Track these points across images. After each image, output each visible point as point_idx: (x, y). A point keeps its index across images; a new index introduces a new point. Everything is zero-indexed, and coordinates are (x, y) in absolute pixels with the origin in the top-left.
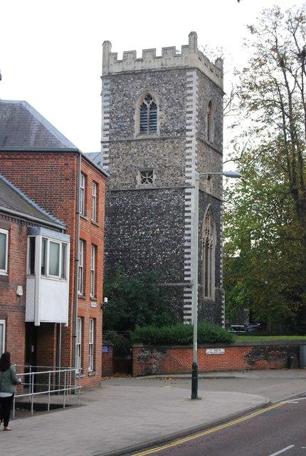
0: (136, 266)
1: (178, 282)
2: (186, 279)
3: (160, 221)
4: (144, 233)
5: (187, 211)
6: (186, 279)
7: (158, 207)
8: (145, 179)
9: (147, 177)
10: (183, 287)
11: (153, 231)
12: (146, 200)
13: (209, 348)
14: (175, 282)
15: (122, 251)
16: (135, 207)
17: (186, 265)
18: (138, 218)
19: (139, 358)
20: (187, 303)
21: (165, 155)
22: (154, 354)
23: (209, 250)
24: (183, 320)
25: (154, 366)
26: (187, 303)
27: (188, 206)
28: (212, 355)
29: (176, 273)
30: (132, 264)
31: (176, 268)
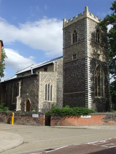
7: (78, 66)
10: (85, 93)
30: (71, 86)
31: (83, 86)
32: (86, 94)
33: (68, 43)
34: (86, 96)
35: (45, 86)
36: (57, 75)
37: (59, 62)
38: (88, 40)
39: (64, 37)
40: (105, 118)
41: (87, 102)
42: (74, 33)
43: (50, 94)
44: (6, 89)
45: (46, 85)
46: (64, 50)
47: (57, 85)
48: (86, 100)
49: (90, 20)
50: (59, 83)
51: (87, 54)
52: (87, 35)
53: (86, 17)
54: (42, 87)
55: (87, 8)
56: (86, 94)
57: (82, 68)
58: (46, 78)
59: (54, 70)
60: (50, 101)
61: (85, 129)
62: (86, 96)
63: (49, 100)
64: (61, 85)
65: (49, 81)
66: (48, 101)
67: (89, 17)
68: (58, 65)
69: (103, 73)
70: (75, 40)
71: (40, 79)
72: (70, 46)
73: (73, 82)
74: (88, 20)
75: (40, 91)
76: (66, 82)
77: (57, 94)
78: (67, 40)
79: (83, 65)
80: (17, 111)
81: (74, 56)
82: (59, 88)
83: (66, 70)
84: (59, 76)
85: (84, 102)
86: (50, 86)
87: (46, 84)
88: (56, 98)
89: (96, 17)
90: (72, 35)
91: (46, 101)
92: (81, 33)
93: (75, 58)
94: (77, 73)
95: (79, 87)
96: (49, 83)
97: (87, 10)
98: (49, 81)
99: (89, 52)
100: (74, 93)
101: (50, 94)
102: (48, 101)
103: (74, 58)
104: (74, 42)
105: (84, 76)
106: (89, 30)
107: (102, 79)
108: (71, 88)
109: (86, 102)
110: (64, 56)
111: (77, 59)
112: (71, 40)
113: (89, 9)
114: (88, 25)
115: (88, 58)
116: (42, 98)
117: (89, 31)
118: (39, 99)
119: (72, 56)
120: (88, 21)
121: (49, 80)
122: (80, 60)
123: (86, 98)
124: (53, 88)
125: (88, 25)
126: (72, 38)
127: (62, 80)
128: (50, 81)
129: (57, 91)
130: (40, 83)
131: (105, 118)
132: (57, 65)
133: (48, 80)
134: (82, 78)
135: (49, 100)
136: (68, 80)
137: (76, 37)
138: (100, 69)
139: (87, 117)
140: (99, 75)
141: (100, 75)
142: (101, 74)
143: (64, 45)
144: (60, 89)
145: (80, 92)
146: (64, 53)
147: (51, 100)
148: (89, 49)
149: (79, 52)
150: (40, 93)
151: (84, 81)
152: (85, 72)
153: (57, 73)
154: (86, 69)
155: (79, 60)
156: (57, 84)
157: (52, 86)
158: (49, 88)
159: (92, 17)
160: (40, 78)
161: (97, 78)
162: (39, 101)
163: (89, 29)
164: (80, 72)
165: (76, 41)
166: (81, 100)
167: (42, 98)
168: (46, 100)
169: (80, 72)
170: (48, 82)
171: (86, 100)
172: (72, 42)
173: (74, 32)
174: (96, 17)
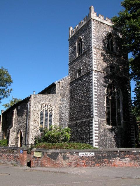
10: (90, 120)
36: (60, 98)
37: (63, 81)
38: (93, 48)
41: (92, 133)
44: (8, 120)
45: (42, 112)
46: (69, 66)
47: (60, 112)
49: (97, 23)
50: (63, 109)
51: (92, 66)
52: (93, 41)
53: (90, 20)
54: (35, 114)
55: (92, 7)
58: (42, 102)
59: (57, 92)
61: (63, 173)
64: (66, 113)
65: (47, 107)
67: (95, 18)
68: (62, 86)
69: (121, 92)
71: (32, 105)
74: (92, 22)
75: (31, 121)
77: (59, 124)
80: (9, 146)
82: (62, 116)
84: (62, 99)
87: (50, 112)
89: (107, 19)
95: (84, 113)
97: (93, 10)
98: (47, 107)
99: (96, 63)
105: (89, 97)
106: (95, 35)
113: (94, 9)
114: (93, 29)
115: (93, 71)
116: (36, 129)
117: (95, 36)
118: (31, 130)
120: (94, 24)
121: (47, 105)
125: (93, 29)
127: (67, 106)
128: (49, 107)
129: (60, 120)
130: (32, 109)
132: (60, 86)
136: (72, 105)
139: (88, 155)
140: (113, 95)
144: (63, 118)
148: (95, 59)
150: (31, 123)
152: (90, 91)
153: (60, 96)
154: (91, 87)
157: (51, 113)
158: (46, 115)
159: (101, 19)
160: (32, 102)
162: (30, 134)
163: (95, 34)
170: (44, 108)
174: (107, 19)
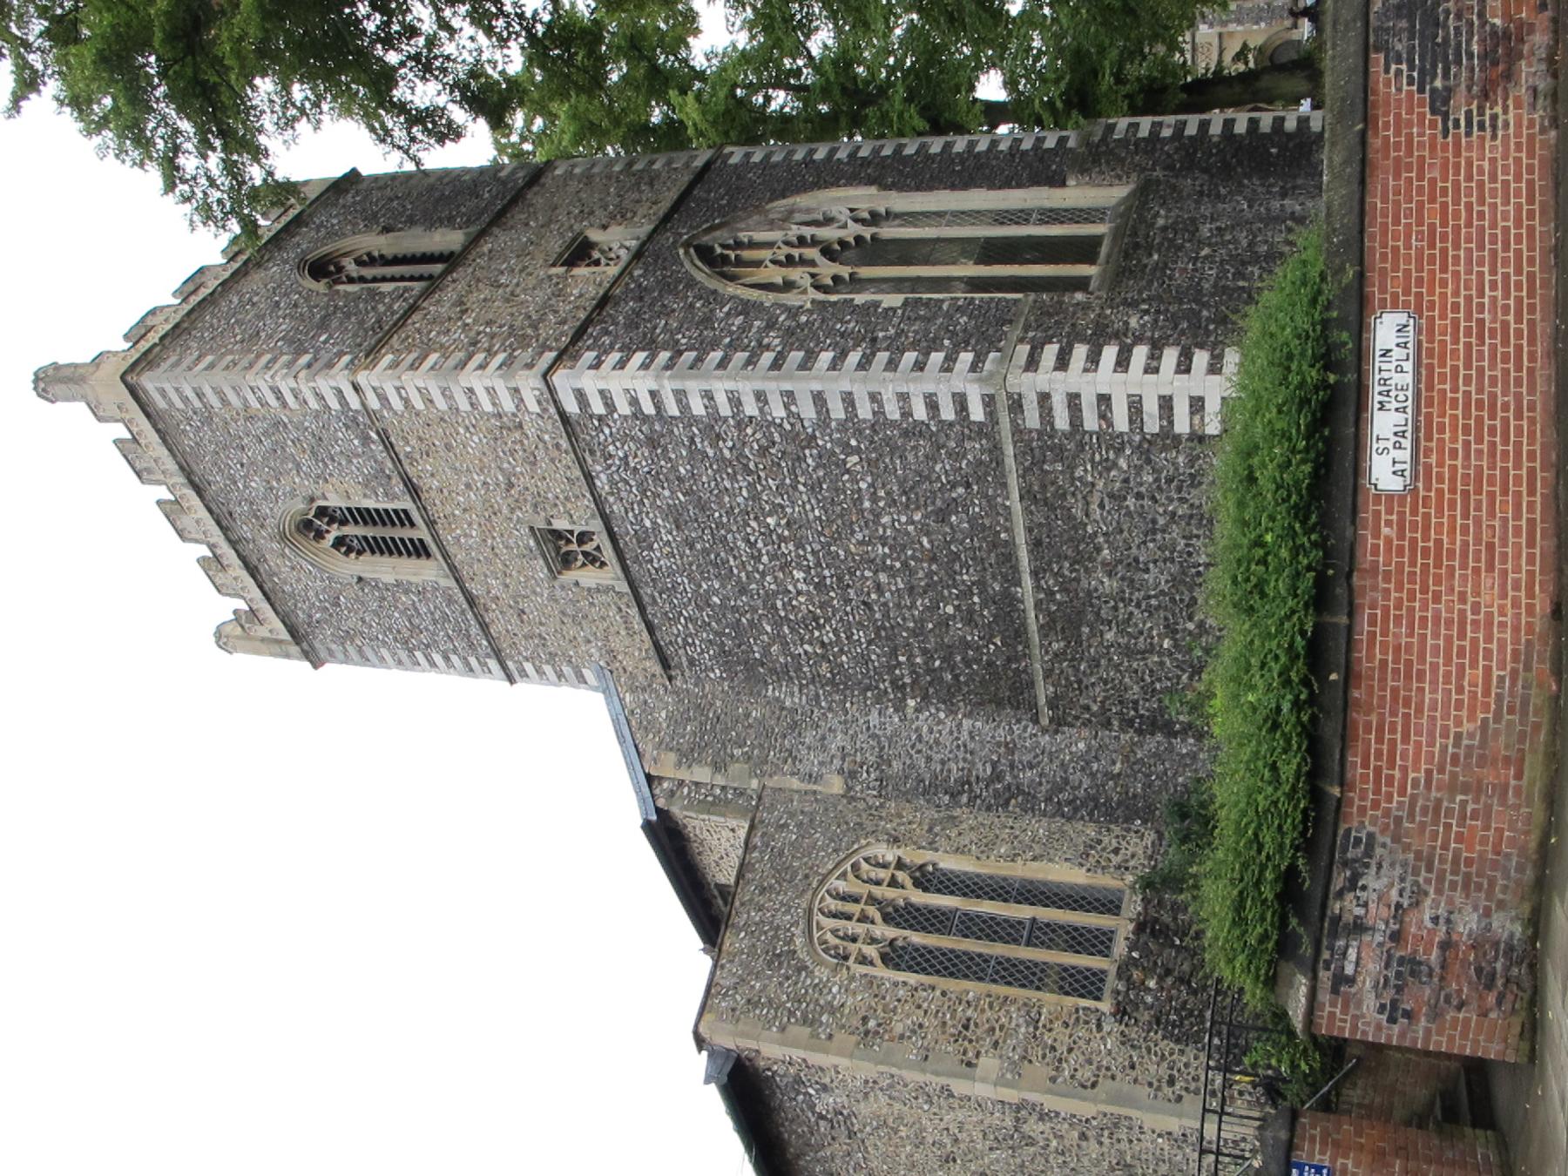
0: (950, 610)
1: (996, 448)
2: (977, 413)
3: (730, 512)
4: (799, 575)
5: (658, 406)
6: (977, 413)
7: (677, 518)
8: (585, 554)
9: (574, 547)
10: (1017, 431)
11: (782, 539)
12: (659, 558)
13: (1358, 467)
14: (1000, 463)
15: (894, 653)
16: (703, 601)
17: (906, 414)
18: (743, 590)
19: (1393, 1012)
20: (1104, 416)
21: (468, 486)
22: (1377, 915)
23: (888, 232)
24: (1199, 438)
25: (1468, 923)
26: (1104, 416)
27: (634, 402)
28: (1422, 431)
29: (956, 456)
30: (944, 622)
31: (932, 458)
32: (1032, 419)
33: (446, 618)
34: (1062, 422)
35: (901, 976)
39: (384, 652)
40: (1426, 75)
42: (330, 538)
43: (1024, 912)
45: (894, 956)
48: (1121, 423)
54: (899, 1028)
56: (1032, 419)
57: (695, 455)
60: (1122, 927)
62: (1062, 422)
63: (1098, 942)
66: (1120, 948)
70: (370, 532)
72: (471, 601)
73: (879, 588)
76: (897, 685)
78: (415, 629)
79: (652, 442)
81: (567, 561)
82: (965, 782)
83: (750, 666)
85: (1161, 458)
86: (919, 898)
88: (1091, 831)
90: (350, 567)
91: (1112, 982)
92: (305, 460)
93: (588, 547)
94: (768, 533)
95: (942, 516)
96: (872, 911)
100: (1028, 582)
101: (1024, 912)
102: (1120, 948)
103: (593, 559)
104: (419, 550)
107: (875, 218)
108: (970, 618)
109: (1152, 426)
110: (587, 673)
111: (596, 525)
112: (398, 584)
116: (1061, 1036)
119: (569, 576)
122: (602, 482)
123: (1091, 422)
124: (950, 863)
126: (385, 569)
131: (1426, 75)
133: (830, 923)
134: (825, 459)
135: (1098, 942)
137: (365, 516)
138: (753, 245)
141: (814, 242)
142: (807, 232)
143: (473, 661)
145: (1015, 503)
146: (560, 675)
147: (1110, 905)
149: (510, 485)
151: (859, 432)
155: (598, 501)
156: (907, 797)
161: (845, 271)
164: (755, 497)
165: (404, 518)
166: (1131, 502)
167: (1061, 1036)
168: (1087, 985)
169: (755, 497)
171: (1121, 423)
172: (427, 572)
173: (320, 535)
